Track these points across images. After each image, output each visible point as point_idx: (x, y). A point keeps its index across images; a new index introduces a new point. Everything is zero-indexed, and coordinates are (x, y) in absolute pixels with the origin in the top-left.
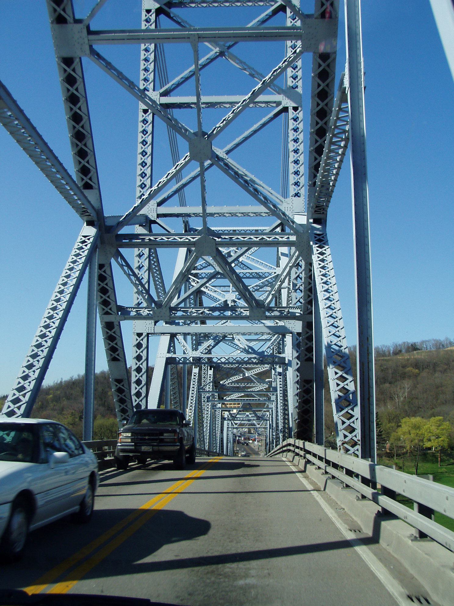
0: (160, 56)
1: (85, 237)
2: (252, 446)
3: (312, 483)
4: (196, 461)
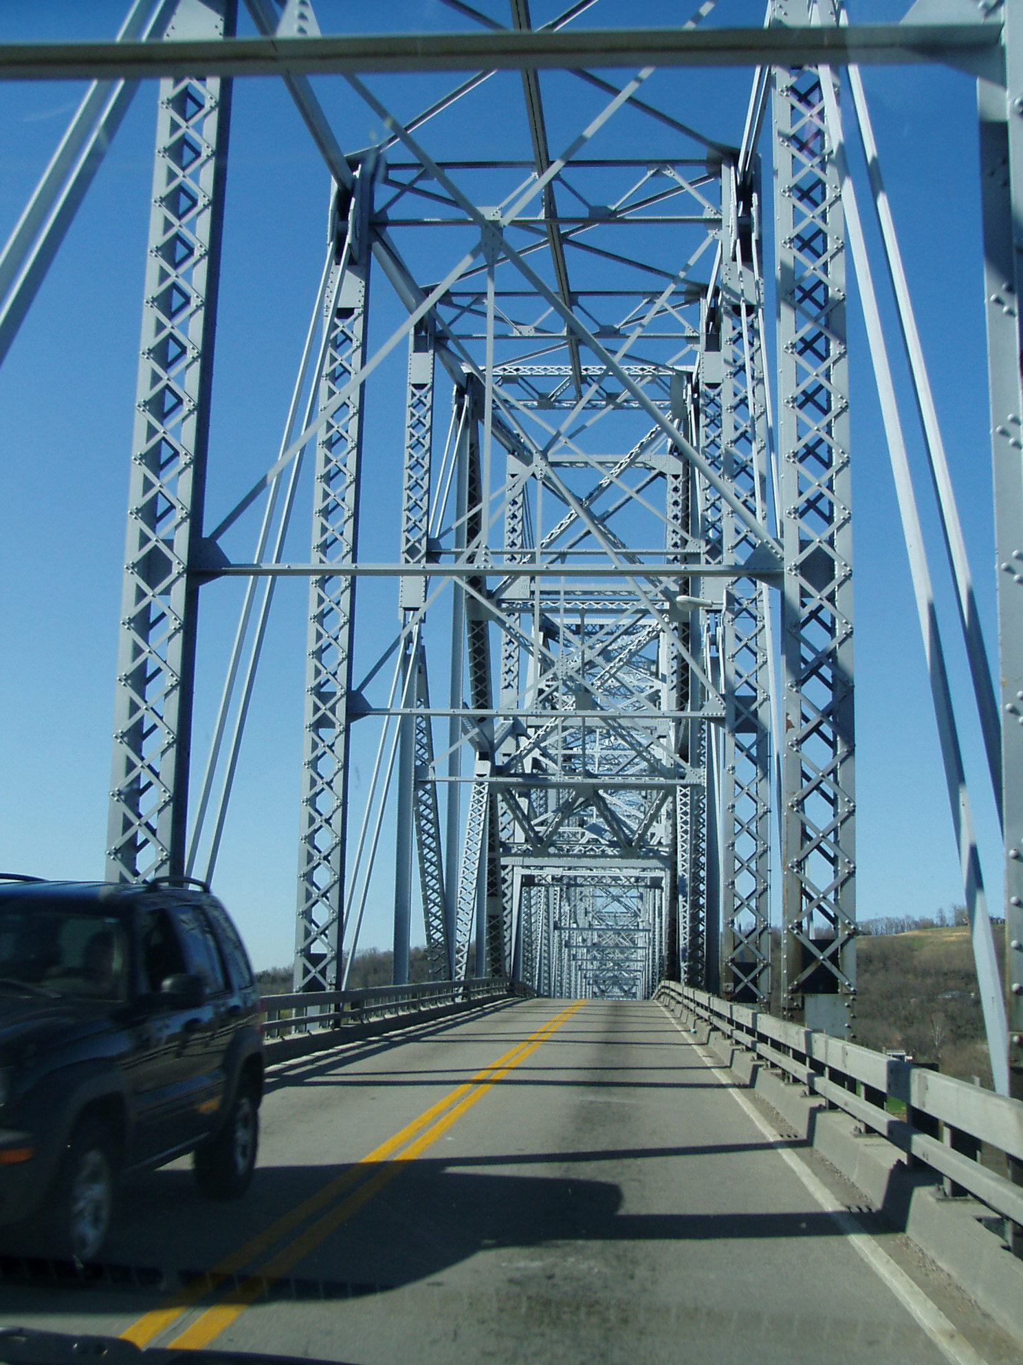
0: (647, 1020)
4: (270, 1155)
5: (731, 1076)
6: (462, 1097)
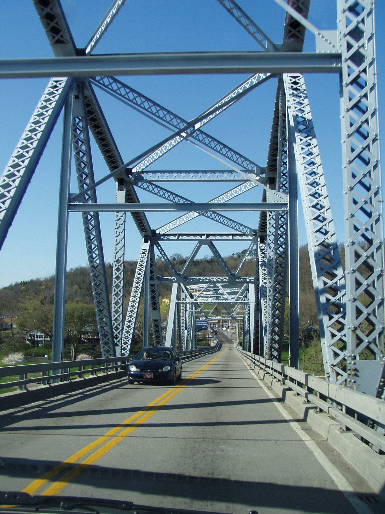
1: (144, 250)
2: (225, 333)
3: (291, 411)
5: (265, 383)
6: (136, 420)
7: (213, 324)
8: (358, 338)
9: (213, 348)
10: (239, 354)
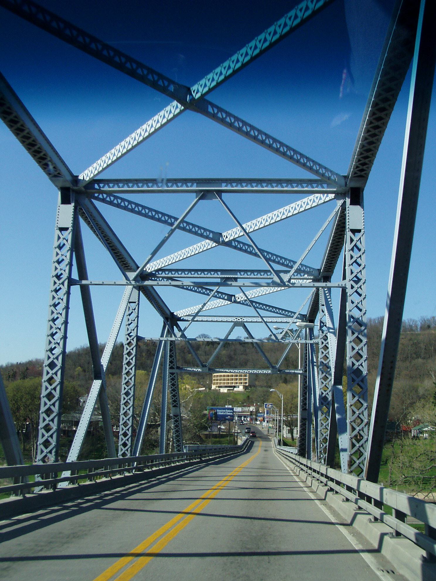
2: (260, 428)
5: (299, 478)
7: (245, 417)
8: (353, 411)
9: (241, 447)
10: (288, 466)
